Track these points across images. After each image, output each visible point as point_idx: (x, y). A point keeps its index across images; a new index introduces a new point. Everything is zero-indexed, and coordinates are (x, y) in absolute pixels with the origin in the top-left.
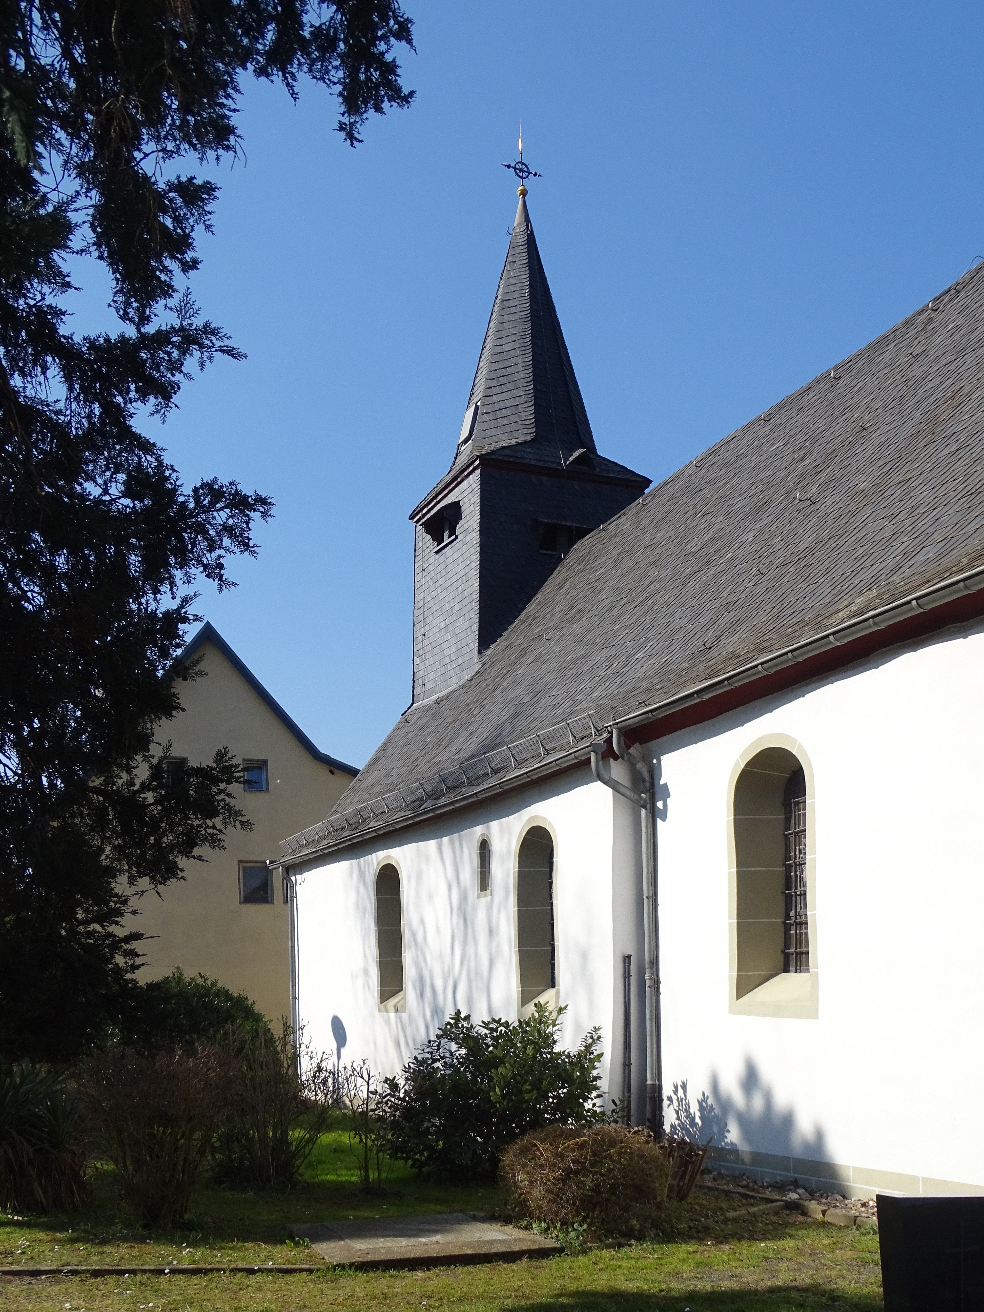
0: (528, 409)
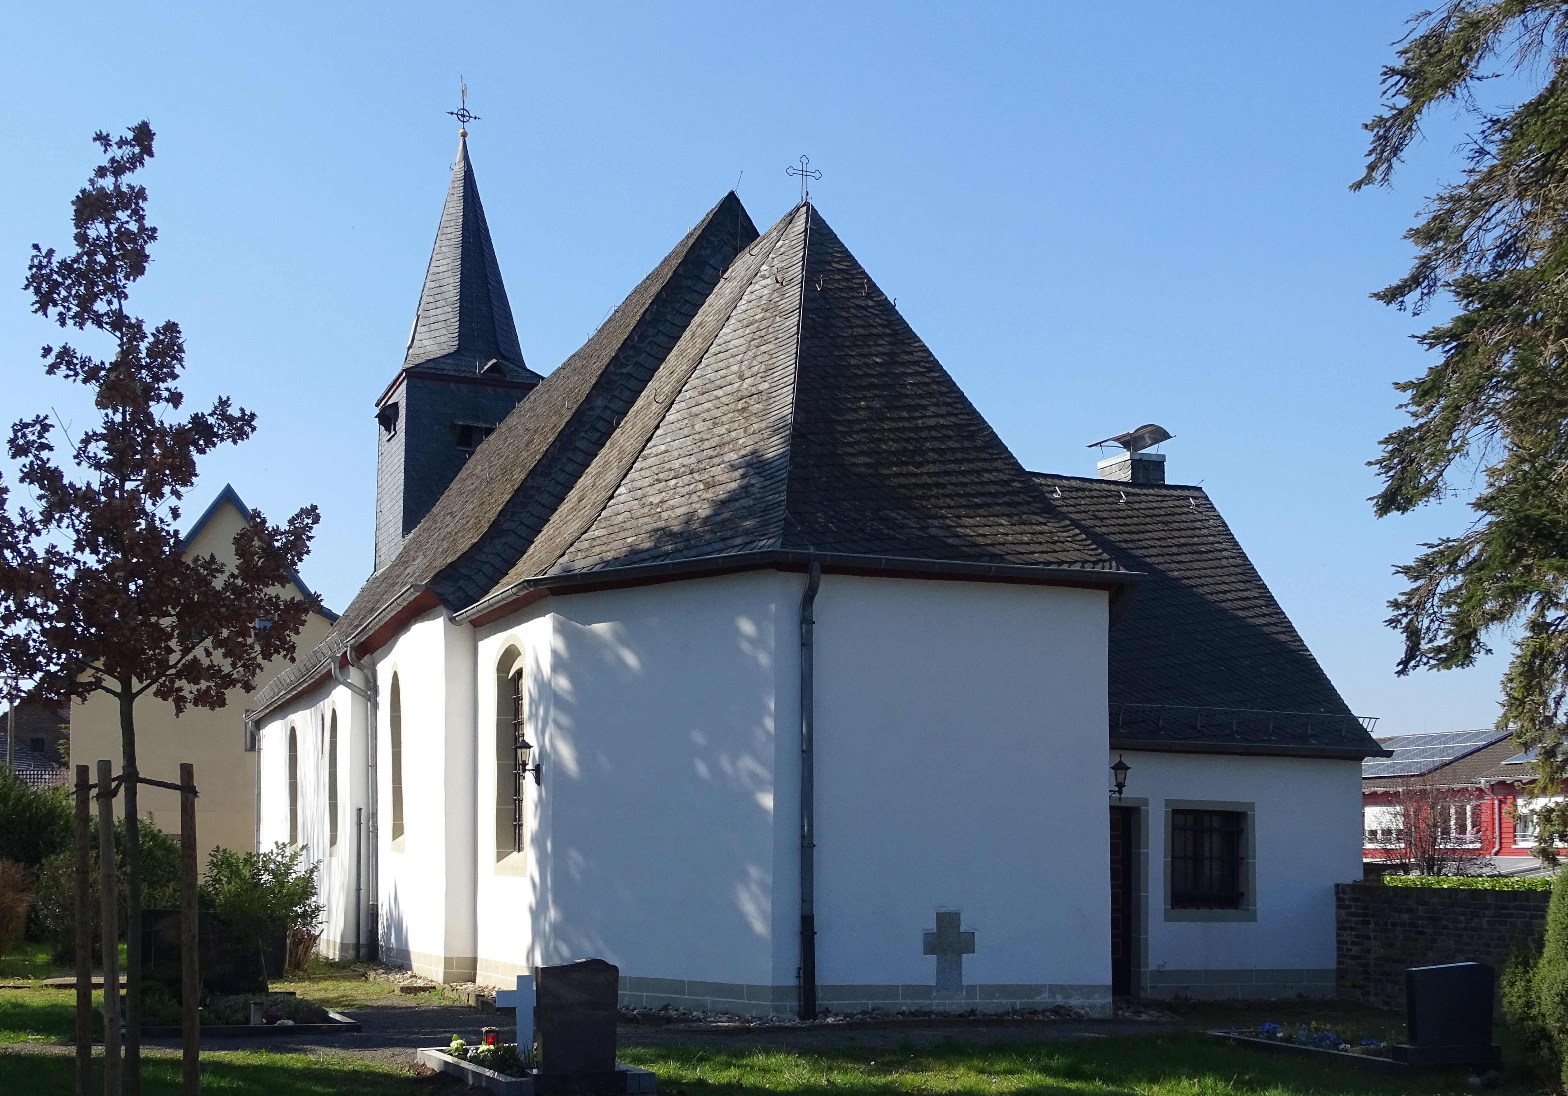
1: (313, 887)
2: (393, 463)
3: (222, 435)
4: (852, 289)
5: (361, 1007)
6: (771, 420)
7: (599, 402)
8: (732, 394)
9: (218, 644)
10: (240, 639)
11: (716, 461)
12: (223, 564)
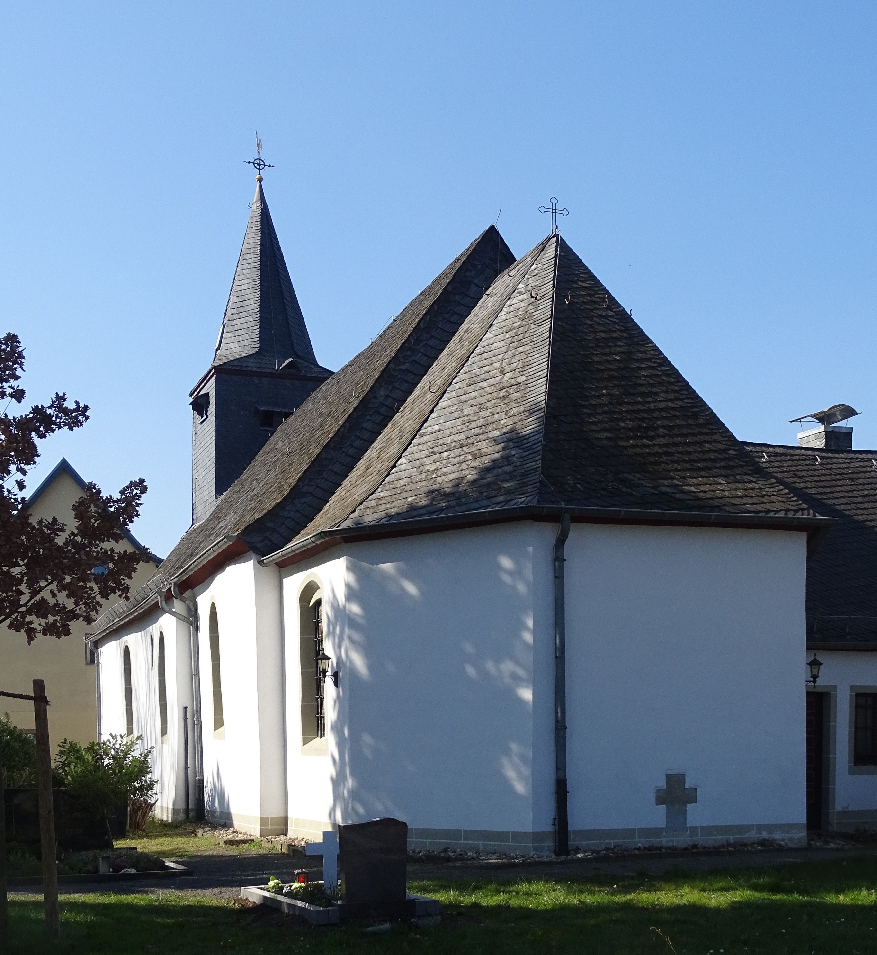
0: (255, 331)
1: (148, 767)
2: (206, 440)
3: (59, 422)
4: (595, 302)
5: (191, 857)
6: (528, 405)
7: (382, 392)
8: (495, 385)
9: (62, 587)
10: (81, 584)
11: (482, 437)
12: (63, 525)
